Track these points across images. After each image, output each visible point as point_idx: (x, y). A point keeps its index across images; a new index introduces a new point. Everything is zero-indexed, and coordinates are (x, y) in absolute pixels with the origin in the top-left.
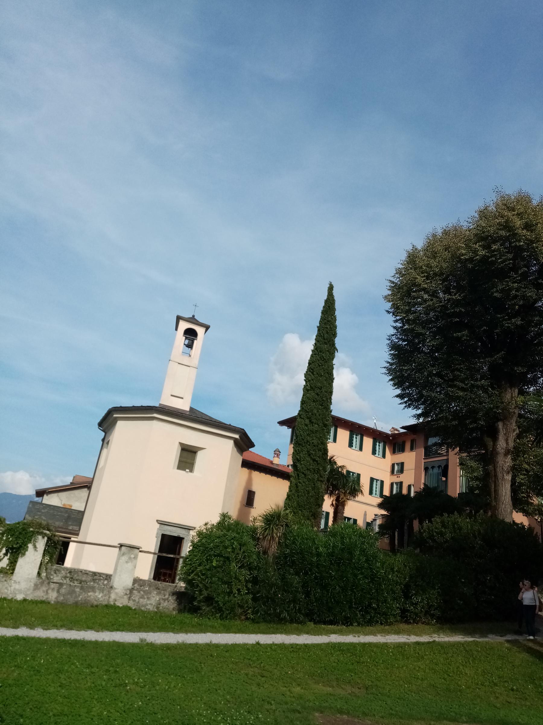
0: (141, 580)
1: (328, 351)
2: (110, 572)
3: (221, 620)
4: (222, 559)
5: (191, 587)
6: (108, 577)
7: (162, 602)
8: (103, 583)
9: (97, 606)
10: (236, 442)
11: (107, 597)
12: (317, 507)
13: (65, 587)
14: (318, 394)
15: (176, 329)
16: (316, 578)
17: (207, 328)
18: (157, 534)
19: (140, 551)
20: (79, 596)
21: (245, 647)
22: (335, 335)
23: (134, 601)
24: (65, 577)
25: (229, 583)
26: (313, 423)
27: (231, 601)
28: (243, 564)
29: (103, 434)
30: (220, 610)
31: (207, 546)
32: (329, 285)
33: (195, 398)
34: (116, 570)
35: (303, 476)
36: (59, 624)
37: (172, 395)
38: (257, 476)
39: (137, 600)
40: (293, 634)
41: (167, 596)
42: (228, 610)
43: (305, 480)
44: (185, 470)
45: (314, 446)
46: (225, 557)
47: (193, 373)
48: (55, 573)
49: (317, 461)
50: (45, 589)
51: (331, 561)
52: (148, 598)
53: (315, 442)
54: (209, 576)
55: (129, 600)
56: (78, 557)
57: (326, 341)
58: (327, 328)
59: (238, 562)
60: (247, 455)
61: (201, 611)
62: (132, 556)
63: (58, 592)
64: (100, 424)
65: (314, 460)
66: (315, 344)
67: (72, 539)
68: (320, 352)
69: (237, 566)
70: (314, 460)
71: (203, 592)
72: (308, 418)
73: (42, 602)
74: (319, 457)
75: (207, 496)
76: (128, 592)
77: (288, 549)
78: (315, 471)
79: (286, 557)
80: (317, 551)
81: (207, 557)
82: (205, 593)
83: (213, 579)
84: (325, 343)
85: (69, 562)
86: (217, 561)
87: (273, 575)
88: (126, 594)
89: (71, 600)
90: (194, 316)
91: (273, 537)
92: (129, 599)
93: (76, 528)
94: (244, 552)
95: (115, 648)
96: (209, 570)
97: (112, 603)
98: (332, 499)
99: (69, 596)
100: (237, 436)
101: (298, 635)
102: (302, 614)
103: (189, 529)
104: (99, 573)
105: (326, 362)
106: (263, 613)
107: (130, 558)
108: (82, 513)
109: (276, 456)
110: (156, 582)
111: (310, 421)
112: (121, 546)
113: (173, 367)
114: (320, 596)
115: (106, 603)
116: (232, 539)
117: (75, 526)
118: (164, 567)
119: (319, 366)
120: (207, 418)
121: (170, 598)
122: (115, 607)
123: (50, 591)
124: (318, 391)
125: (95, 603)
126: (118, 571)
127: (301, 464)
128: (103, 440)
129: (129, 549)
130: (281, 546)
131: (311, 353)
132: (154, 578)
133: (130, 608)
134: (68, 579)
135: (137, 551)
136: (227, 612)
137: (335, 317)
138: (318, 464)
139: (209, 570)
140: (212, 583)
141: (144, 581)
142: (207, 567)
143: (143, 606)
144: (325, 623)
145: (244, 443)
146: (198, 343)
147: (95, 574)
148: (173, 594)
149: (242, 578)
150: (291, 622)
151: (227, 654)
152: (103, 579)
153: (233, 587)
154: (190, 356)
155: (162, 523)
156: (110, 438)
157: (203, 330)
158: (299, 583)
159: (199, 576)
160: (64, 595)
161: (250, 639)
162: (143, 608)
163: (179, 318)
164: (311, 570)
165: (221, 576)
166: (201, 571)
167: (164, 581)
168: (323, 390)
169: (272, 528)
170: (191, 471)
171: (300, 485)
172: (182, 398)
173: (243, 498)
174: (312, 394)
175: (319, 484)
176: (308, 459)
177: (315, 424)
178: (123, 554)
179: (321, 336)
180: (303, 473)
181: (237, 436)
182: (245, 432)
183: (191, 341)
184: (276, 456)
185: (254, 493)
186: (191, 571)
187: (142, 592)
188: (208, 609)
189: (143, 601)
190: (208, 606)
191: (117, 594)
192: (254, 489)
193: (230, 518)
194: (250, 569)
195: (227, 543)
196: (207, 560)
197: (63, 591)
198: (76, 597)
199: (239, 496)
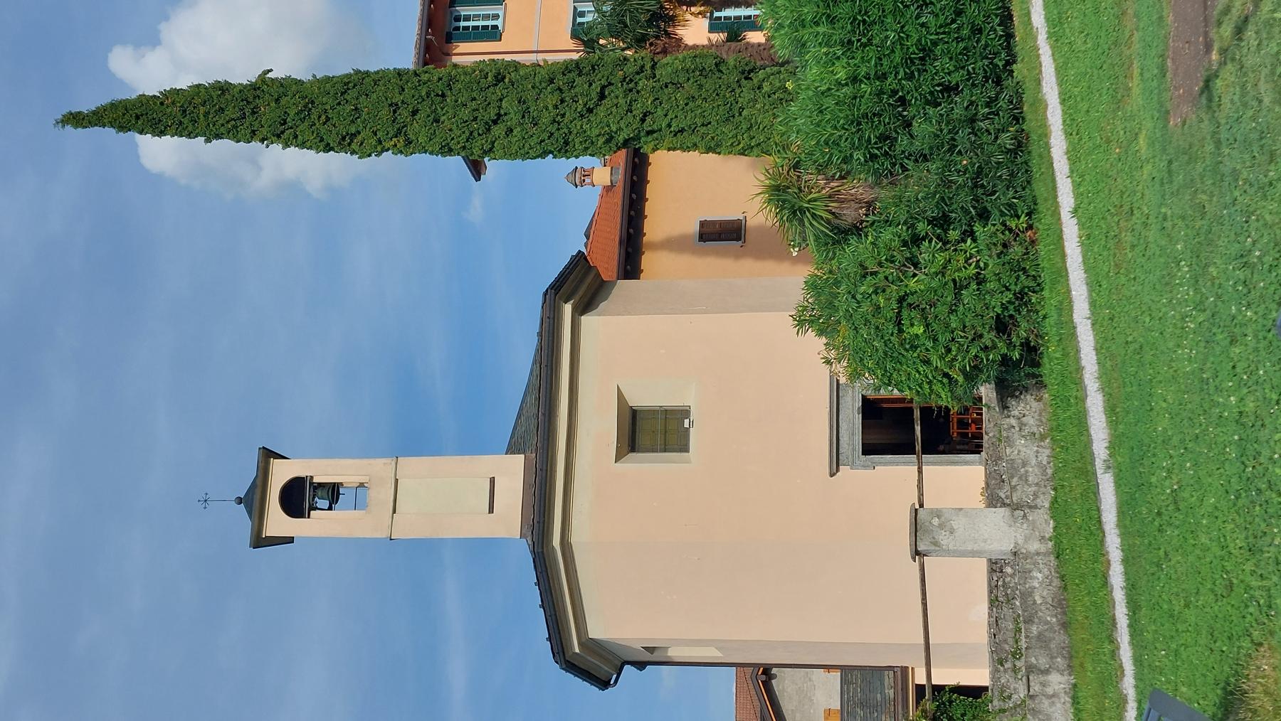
0: (987, 484)
1: (277, 101)
2: (982, 566)
3: (1042, 290)
4: (905, 313)
5: (981, 371)
6: (995, 567)
7: (1027, 430)
8: (1013, 576)
9: (1062, 578)
10: (585, 307)
11: (1039, 559)
12: (723, 68)
13: (1033, 660)
14: (414, 113)
15: (290, 540)
16: (910, 77)
17: (268, 455)
18: (865, 467)
19: (921, 506)
20: (1047, 623)
21: (1087, 241)
22: (223, 88)
23: (1035, 495)
24: (1015, 670)
25: (958, 287)
26: (499, 115)
27: (996, 275)
28: (907, 259)
29: (627, 667)
30: (1021, 296)
31: (881, 353)
32: (69, 128)
33: (471, 445)
34: (974, 554)
35: (648, 120)
36: (1107, 647)
37: (491, 510)
38: (656, 225)
39: (1034, 489)
40: (1046, 118)
41: (1013, 422)
42: (1018, 278)
43: (660, 112)
44: (688, 429)
45: (562, 101)
46: (900, 308)
47: (410, 465)
48: (1010, 697)
49: (603, 88)
50: (1046, 702)
51: (864, 45)
52: (1024, 464)
53: (552, 100)
54: (949, 336)
55: (1036, 507)
56: (961, 656)
57: (248, 111)
58: (206, 114)
59: (904, 273)
60: (607, 261)
61: (1032, 337)
62: (936, 521)
63: (1046, 672)
64: (604, 684)
65: (602, 96)
66: (262, 141)
67: (921, 679)
68: (285, 123)
69: (915, 275)
70: (602, 96)
71: (989, 344)
72: (489, 130)
73: (1075, 701)
74: (591, 85)
75: (736, 347)
76: (1019, 513)
77: (851, 155)
78: (631, 90)
79: (874, 157)
80: (847, 84)
81: (907, 350)
82: (989, 338)
83: (954, 325)
84: (253, 113)
85: (979, 676)
86: (912, 325)
87: (920, 183)
88: (1025, 516)
89: (1060, 638)
90: (239, 500)
91: (830, 197)
92: (1033, 508)
93: (888, 679)
94: (880, 265)
95: (1128, 522)
96: (935, 340)
97: (1050, 544)
98: (688, 16)
99: (1052, 646)
100: (568, 308)
101: (1047, 106)
102: (998, 94)
103: (837, 389)
104: (991, 592)
105: (313, 102)
106: (1011, 193)
107: (941, 526)
108: (847, 672)
109: (588, 180)
110: (985, 445)
111: (495, 122)
112: (917, 553)
113: (407, 528)
114: (951, 59)
115: (1052, 558)
116: (854, 297)
117: (882, 684)
118: (948, 434)
119: (328, 119)
120: (532, 399)
121: (1016, 413)
122: (1057, 538)
123: (1050, 691)
124: (404, 114)
125: (1057, 582)
126: (976, 548)
127: (620, 129)
128: (641, 665)
129: (922, 535)
130: (848, 173)
131: (292, 150)
132: (977, 449)
133: (1054, 501)
134: (1018, 664)
135: (921, 511)
136: (1023, 277)
137: (166, 94)
138: (610, 84)
139: (935, 340)
140: (965, 327)
141: (988, 476)
142: (930, 344)
143: (1044, 472)
144: (1009, 36)
145: (579, 286)
146: (321, 471)
147: (994, 602)
148: (1005, 407)
149: (940, 258)
150: (1018, 119)
151: (1105, 284)
152: (1002, 576)
153: (964, 274)
154: (362, 485)
155: (836, 463)
156: (638, 646)
157: (276, 464)
158: (927, 119)
159: (954, 360)
160: (1052, 658)
161: (1071, 231)
162: (1050, 471)
163: (260, 541)
164: (895, 92)
165: (945, 309)
166: (942, 358)
167: (979, 422)
168: (398, 99)
169: (809, 202)
170: (685, 413)
171: (674, 124)
172: (492, 481)
173: (718, 254)
174: (417, 129)
175: (663, 73)
176: (601, 111)
177: (500, 107)
178: (936, 544)
179: (235, 127)
180: (643, 120)
181: (568, 308)
182: (552, 287)
183: (319, 492)
184: (588, 180)
185: (702, 224)
186: (945, 380)
187: (1015, 481)
188: (1024, 325)
189: (1034, 475)
190: (1016, 325)
191: (1027, 539)
192: (695, 228)
193: (805, 308)
194: (917, 240)
195: (866, 307)
196: (914, 348)
197: (1043, 662)
198: (1051, 629)
199: (719, 267)
